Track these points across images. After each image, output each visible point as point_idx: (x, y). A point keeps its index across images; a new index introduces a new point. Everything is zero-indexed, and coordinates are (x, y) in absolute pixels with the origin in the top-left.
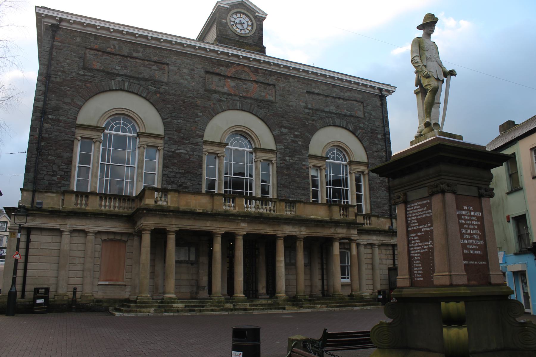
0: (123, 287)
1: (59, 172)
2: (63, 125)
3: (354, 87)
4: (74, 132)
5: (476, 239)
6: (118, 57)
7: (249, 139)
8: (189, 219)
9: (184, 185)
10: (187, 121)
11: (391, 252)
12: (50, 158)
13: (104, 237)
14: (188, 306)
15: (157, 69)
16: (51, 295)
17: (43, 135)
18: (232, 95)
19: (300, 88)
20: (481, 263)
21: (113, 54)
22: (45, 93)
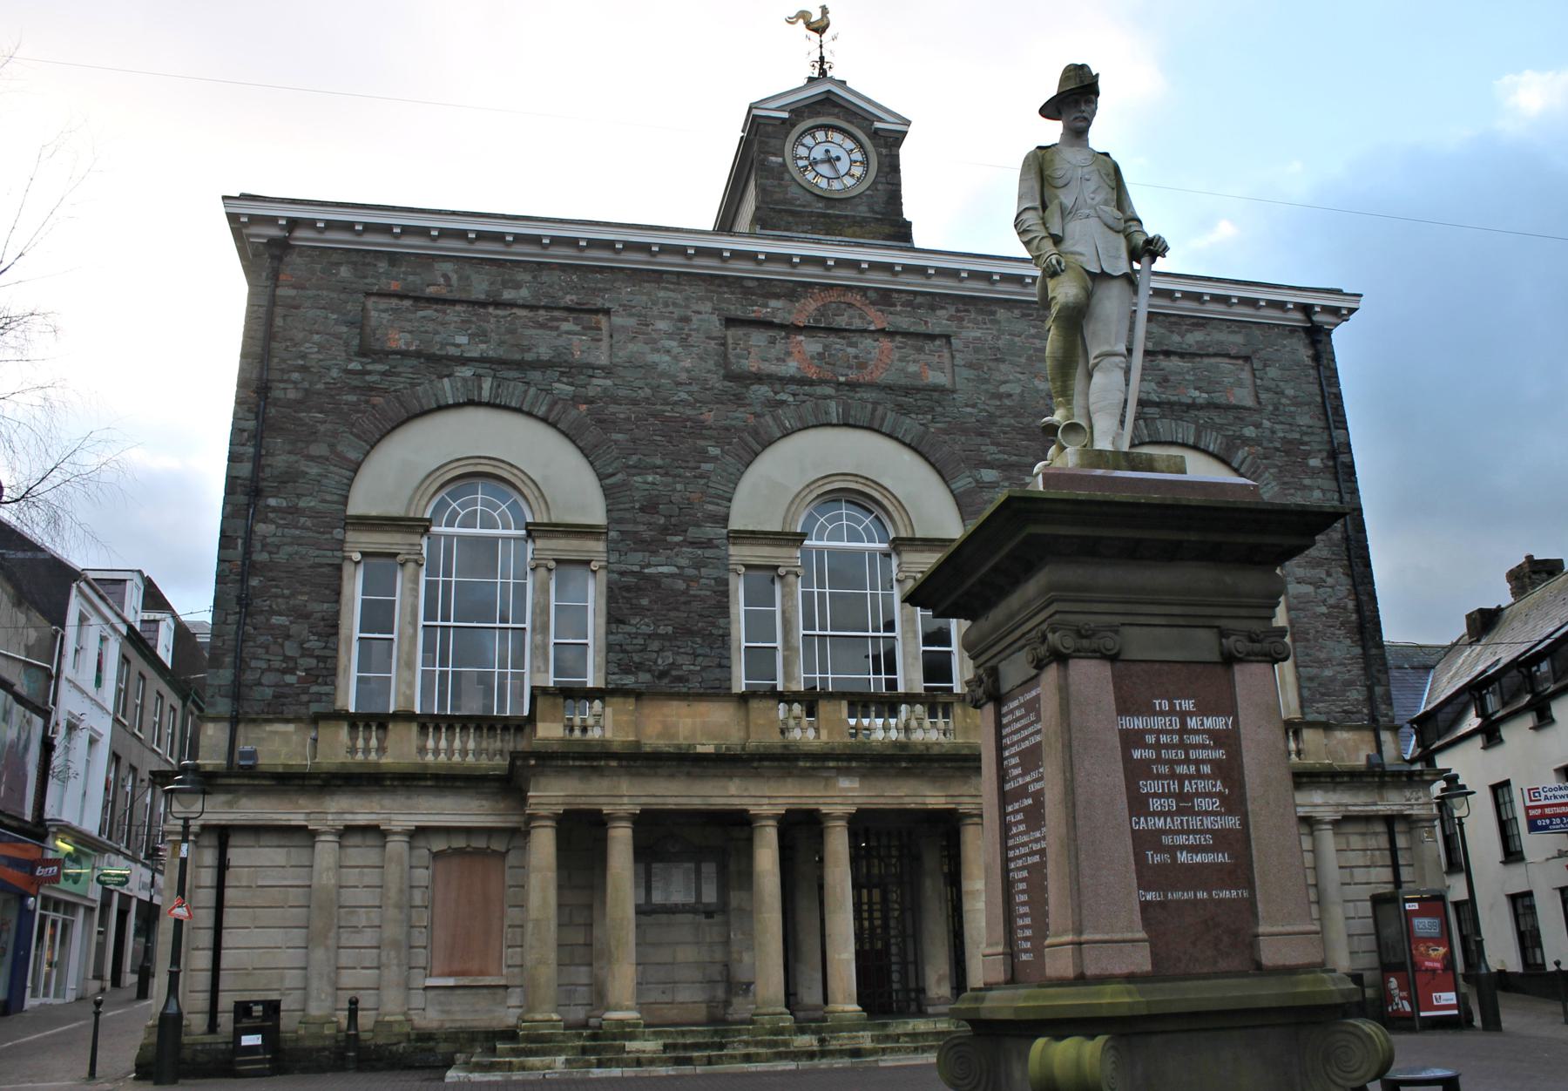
0: (501, 991)
1: (301, 661)
2: (309, 524)
3: (1215, 311)
4: (342, 542)
5: (1207, 813)
6: (458, 308)
7: (877, 511)
8: (672, 776)
9: (674, 673)
10: (675, 476)
11: (1383, 841)
12: (275, 620)
13: (439, 845)
14: (674, 1047)
15: (578, 328)
16: (288, 1022)
17: (255, 557)
18: (811, 383)
19: (1034, 337)
20: (1225, 894)
21: (445, 301)
22: (258, 437)
